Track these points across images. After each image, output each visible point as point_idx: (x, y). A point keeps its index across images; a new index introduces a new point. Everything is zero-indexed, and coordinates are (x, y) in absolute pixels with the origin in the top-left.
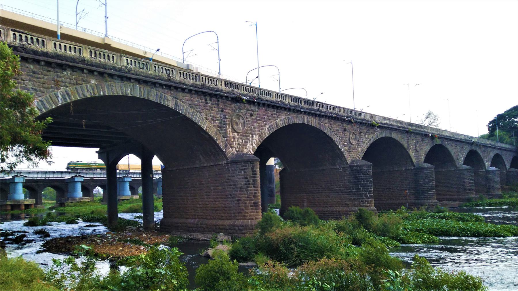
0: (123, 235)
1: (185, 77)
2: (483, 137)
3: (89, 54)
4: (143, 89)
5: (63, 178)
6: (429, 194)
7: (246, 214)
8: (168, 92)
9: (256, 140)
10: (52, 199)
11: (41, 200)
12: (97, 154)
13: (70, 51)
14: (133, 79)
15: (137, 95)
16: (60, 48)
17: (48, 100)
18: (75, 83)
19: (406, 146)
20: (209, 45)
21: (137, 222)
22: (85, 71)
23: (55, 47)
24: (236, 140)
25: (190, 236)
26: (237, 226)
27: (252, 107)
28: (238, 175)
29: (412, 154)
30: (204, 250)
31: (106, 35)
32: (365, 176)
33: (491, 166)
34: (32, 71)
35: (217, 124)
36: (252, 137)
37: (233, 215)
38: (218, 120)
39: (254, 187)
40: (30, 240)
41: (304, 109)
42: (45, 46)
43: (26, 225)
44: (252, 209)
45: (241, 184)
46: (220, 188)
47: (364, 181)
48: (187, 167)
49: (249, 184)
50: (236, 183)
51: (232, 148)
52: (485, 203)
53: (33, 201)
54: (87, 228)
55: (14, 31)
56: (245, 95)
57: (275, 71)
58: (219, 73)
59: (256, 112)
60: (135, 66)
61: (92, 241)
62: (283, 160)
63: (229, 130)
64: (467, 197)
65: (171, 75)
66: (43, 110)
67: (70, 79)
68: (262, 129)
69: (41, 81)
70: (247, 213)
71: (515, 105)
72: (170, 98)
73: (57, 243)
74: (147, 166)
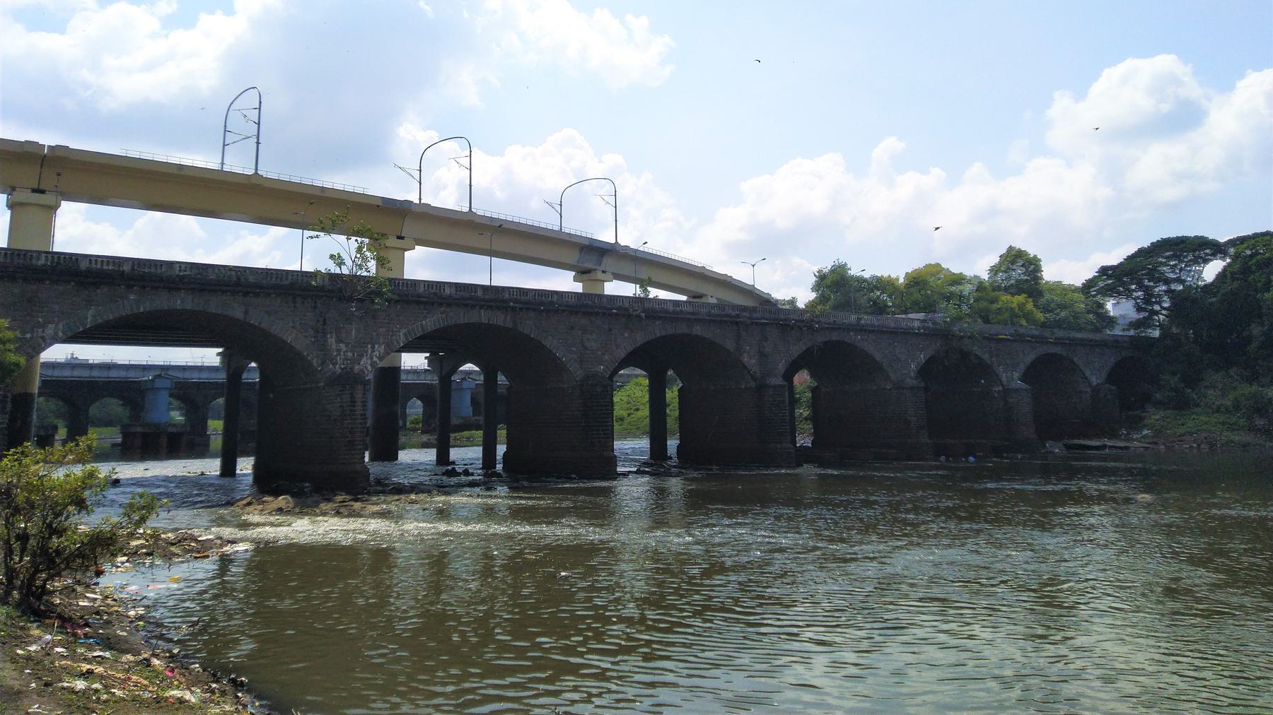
9: (379, 352)
24: (342, 353)
36: (373, 347)
57: (608, 187)
71: (1200, 234)
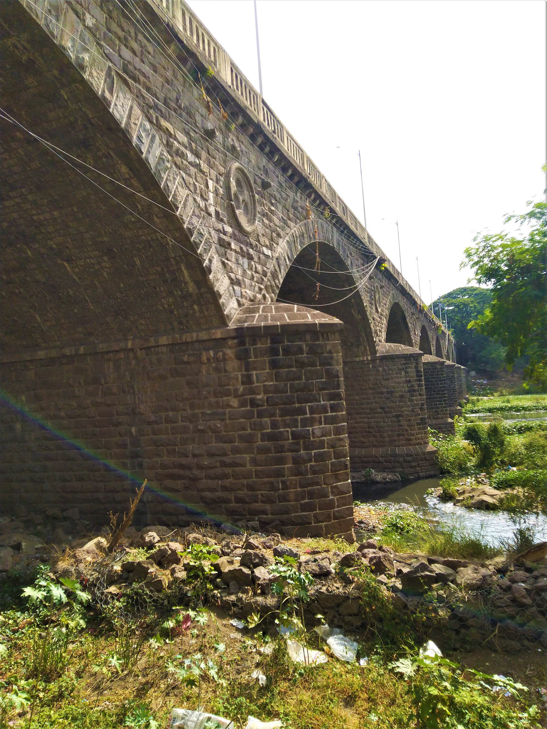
7: (412, 437)
26: (401, 456)
28: (396, 377)
32: (438, 378)
37: (387, 439)
44: (419, 429)
47: (438, 384)
49: (414, 391)
50: (393, 389)
70: (413, 435)
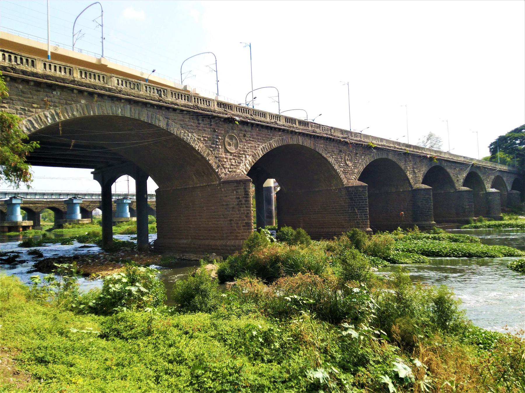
0: (116, 255)
1: (177, 98)
2: (486, 159)
3: (79, 74)
4: (134, 110)
5: (61, 200)
6: (427, 215)
7: (238, 235)
8: (159, 112)
10: (53, 222)
11: (39, 221)
12: (92, 175)
13: (60, 71)
14: (123, 99)
15: (128, 115)
16: (50, 69)
17: (37, 119)
18: (65, 103)
19: (403, 168)
20: (207, 66)
21: (132, 243)
22: (75, 91)
23: (45, 68)
25: (183, 256)
27: (246, 128)
29: (410, 176)
30: (193, 270)
31: (102, 56)
32: (361, 197)
33: (492, 188)
34: (21, 91)
35: (209, 144)
36: (246, 157)
37: (225, 235)
38: (210, 140)
39: (246, 207)
40: (22, 261)
41: (299, 129)
42: (35, 66)
43: (20, 246)
44: (244, 229)
45: (233, 204)
46: (213, 208)
47: (359, 202)
48: (180, 188)
49: (242, 204)
50: (228, 203)
51: (224, 168)
52: (484, 225)
53: (30, 223)
54: (82, 249)
55: (3, 51)
56: (238, 116)
58: (218, 94)
59: (250, 133)
60: (126, 86)
61: (84, 261)
62: (279, 181)
63: (222, 150)
64: (466, 218)
65: (163, 96)
66: (32, 129)
67: (59, 99)
68: (256, 150)
69: (31, 100)
70: (239, 233)
72: (161, 118)
73: (48, 263)
74: (141, 187)
